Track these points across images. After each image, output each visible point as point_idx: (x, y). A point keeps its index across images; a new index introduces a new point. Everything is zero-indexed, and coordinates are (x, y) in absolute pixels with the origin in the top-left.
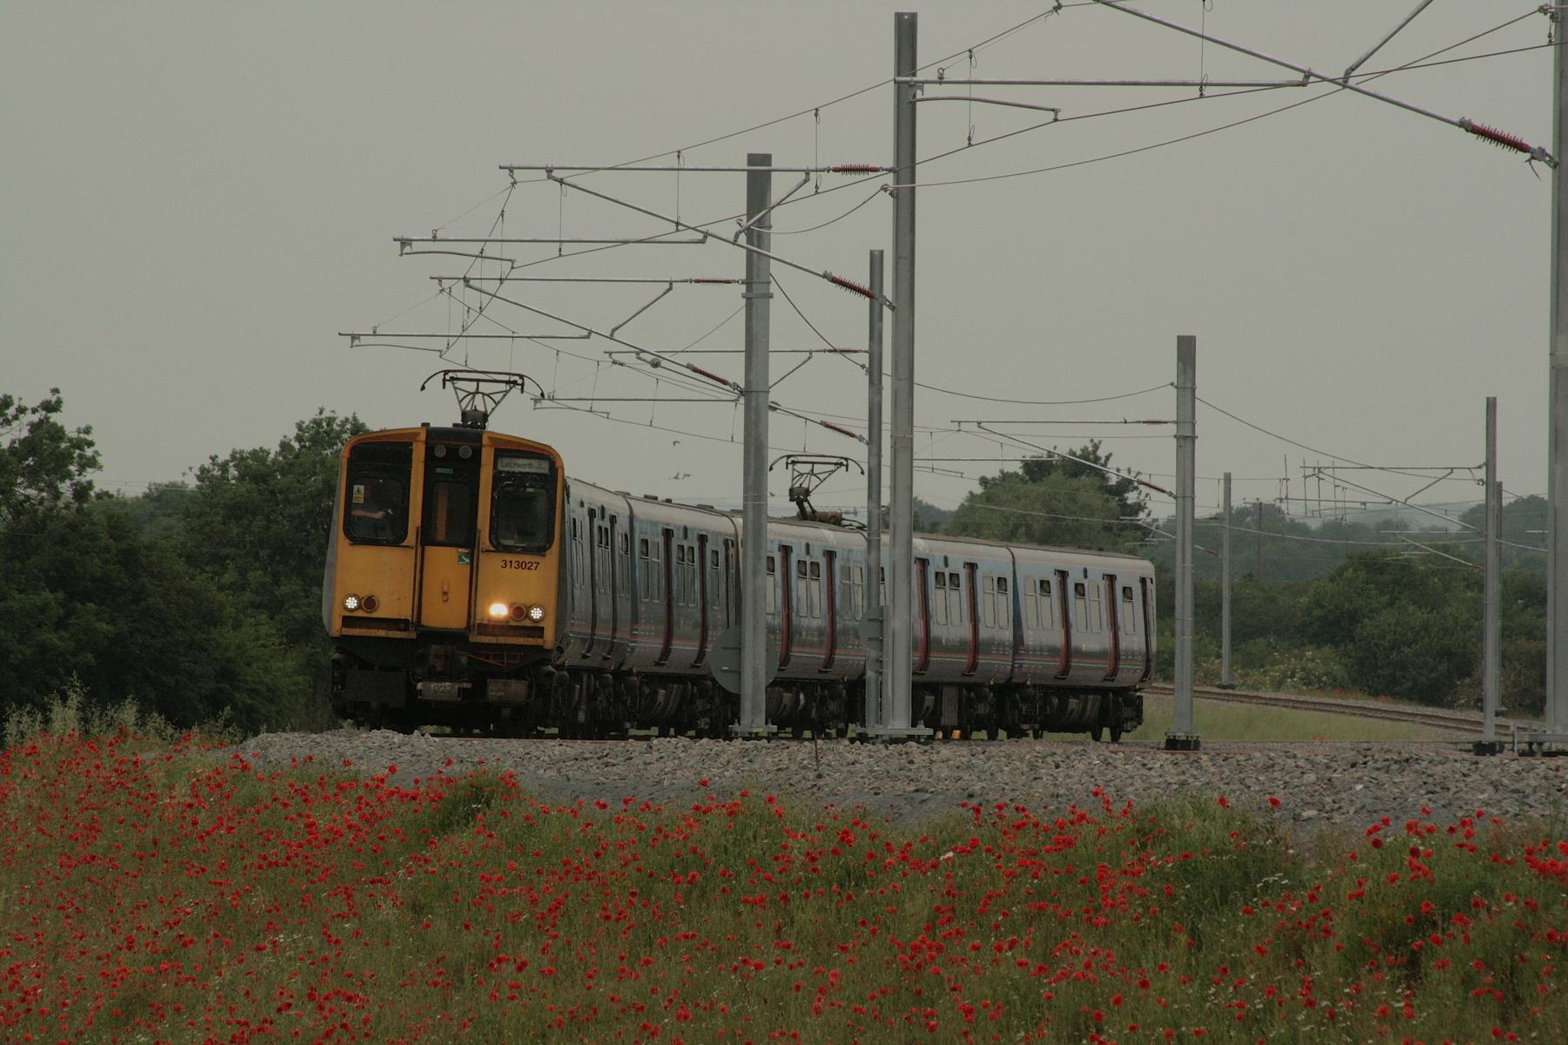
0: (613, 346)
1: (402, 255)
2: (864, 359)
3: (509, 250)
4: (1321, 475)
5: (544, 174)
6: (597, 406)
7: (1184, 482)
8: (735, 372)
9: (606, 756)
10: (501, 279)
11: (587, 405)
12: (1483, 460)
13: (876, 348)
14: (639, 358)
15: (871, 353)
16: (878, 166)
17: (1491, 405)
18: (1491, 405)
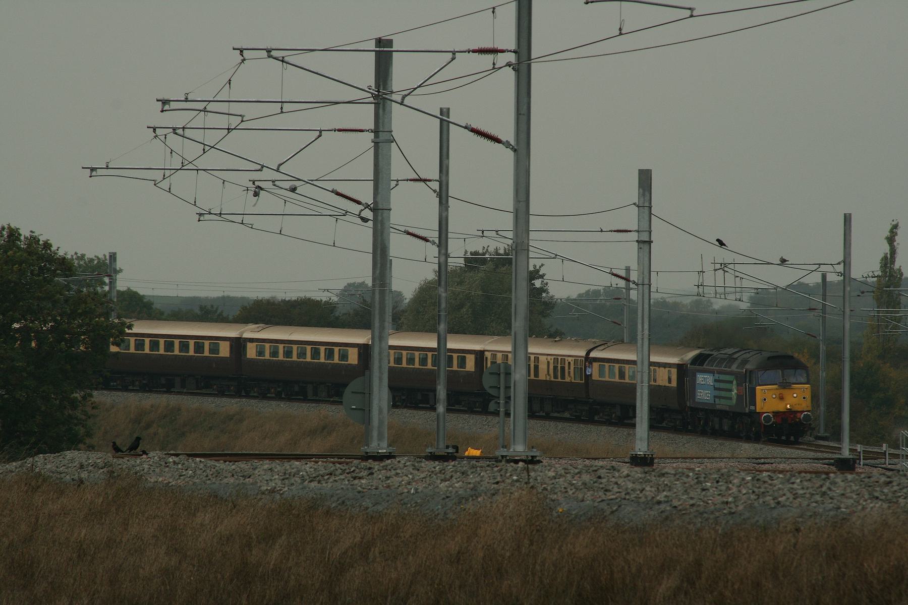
0: (277, 176)
1: (162, 111)
2: (436, 186)
3: (235, 108)
4: (726, 269)
5: (265, 54)
6: (247, 220)
7: (643, 274)
8: (366, 194)
9: (352, 472)
10: (228, 129)
11: (238, 219)
12: (842, 259)
13: (444, 178)
14: (274, 185)
15: (440, 182)
16: (504, 49)
17: (847, 219)
18: (847, 219)
